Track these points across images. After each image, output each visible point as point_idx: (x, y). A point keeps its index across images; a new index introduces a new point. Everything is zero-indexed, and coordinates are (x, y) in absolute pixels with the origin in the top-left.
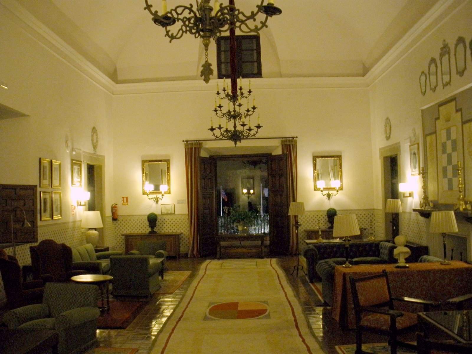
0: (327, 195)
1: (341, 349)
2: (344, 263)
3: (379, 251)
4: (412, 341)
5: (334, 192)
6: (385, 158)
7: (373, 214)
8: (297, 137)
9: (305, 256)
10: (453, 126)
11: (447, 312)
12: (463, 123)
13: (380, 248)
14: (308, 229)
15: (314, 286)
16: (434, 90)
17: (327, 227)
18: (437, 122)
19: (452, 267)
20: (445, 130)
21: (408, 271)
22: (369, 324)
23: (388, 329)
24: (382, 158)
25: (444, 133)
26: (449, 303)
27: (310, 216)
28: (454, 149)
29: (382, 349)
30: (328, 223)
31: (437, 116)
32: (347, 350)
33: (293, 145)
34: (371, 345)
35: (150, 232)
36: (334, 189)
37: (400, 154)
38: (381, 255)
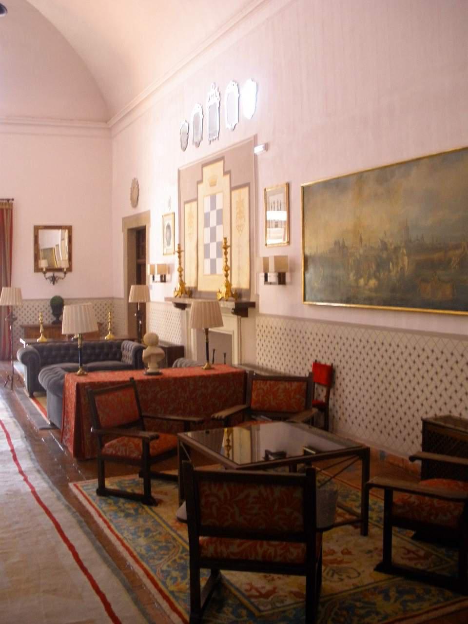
0: (51, 279)
1: (77, 487)
2: (75, 370)
3: (121, 354)
4: (170, 469)
5: (61, 275)
6: (130, 231)
7: (111, 304)
8: (13, 200)
9: (24, 361)
10: (219, 192)
11: (210, 430)
12: (232, 189)
13: (122, 349)
14: (25, 323)
15: (38, 403)
16: (198, 145)
17: (51, 321)
18: (200, 186)
19: (217, 372)
20: (209, 197)
21: (162, 379)
22: (114, 452)
23: (140, 457)
24: (126, 231)
25: (208, 201)
26: (214, 419)
27: (28, 306)
28: (220, 221)
29: (132, 483)
30: (52, 316)
31: (200, 179)
32: (85, 488)
33: (7, 210)
34: (116, 479)
35: (54, 323)
36: (60, 270)
37: (150, 226)
38: (124, 359)
